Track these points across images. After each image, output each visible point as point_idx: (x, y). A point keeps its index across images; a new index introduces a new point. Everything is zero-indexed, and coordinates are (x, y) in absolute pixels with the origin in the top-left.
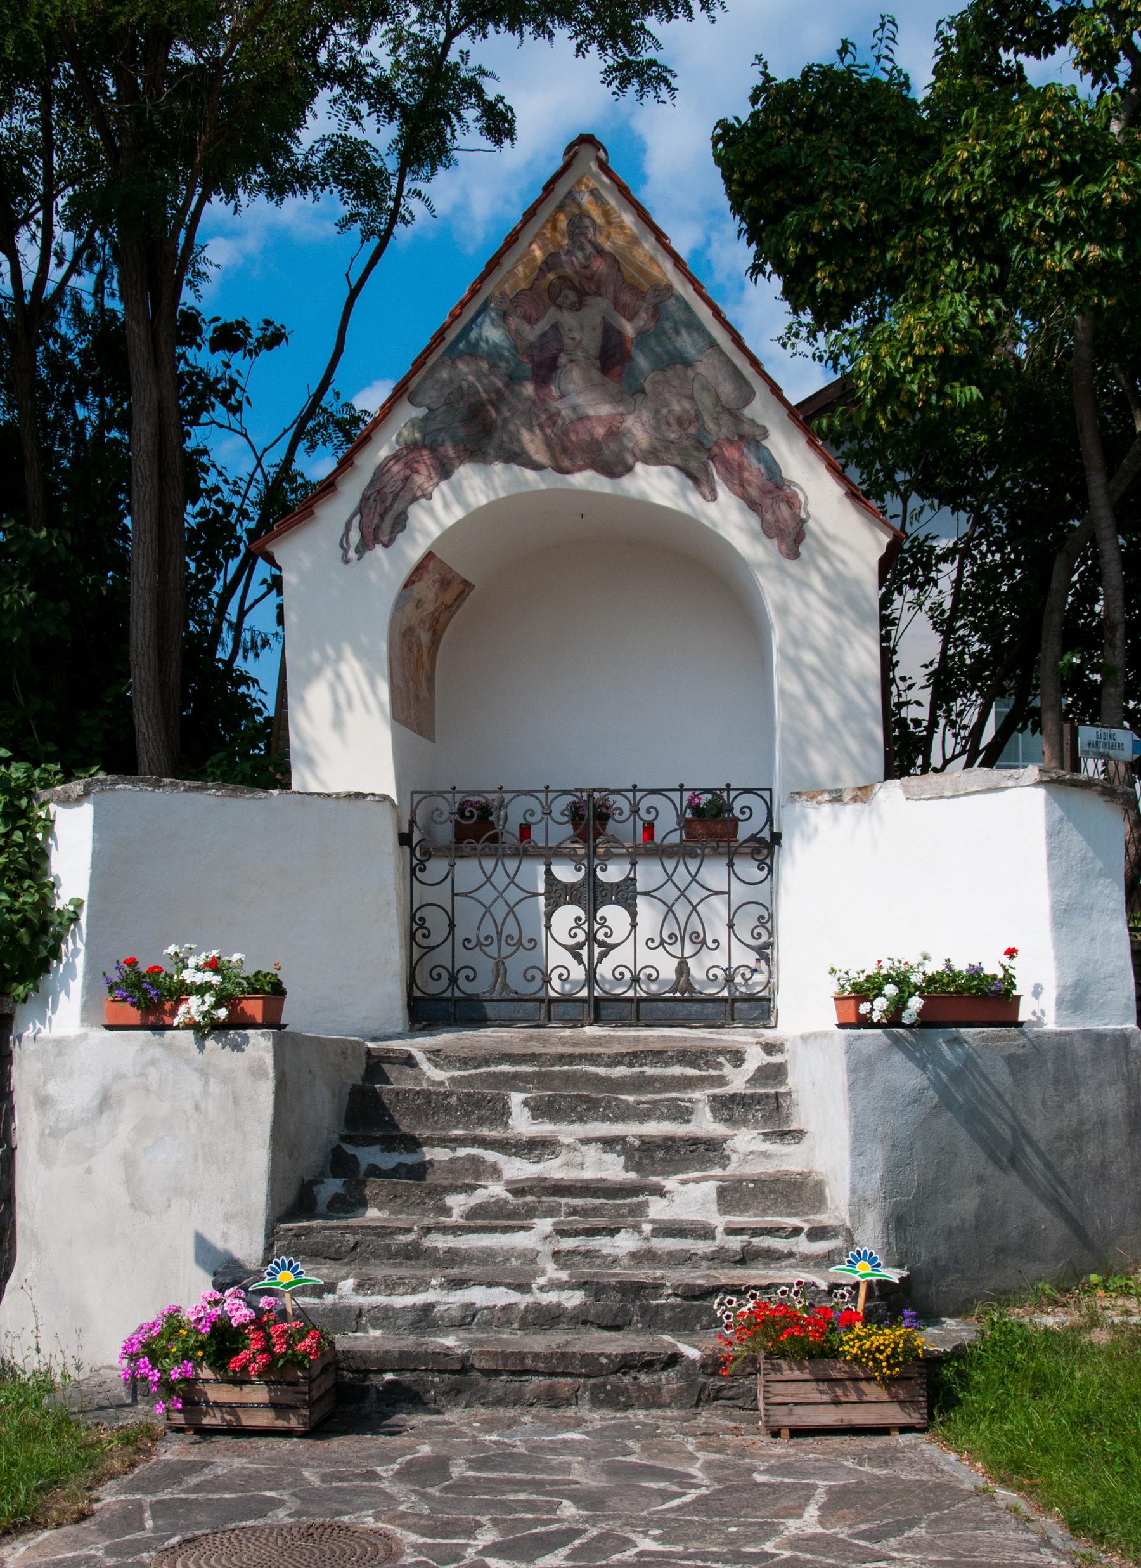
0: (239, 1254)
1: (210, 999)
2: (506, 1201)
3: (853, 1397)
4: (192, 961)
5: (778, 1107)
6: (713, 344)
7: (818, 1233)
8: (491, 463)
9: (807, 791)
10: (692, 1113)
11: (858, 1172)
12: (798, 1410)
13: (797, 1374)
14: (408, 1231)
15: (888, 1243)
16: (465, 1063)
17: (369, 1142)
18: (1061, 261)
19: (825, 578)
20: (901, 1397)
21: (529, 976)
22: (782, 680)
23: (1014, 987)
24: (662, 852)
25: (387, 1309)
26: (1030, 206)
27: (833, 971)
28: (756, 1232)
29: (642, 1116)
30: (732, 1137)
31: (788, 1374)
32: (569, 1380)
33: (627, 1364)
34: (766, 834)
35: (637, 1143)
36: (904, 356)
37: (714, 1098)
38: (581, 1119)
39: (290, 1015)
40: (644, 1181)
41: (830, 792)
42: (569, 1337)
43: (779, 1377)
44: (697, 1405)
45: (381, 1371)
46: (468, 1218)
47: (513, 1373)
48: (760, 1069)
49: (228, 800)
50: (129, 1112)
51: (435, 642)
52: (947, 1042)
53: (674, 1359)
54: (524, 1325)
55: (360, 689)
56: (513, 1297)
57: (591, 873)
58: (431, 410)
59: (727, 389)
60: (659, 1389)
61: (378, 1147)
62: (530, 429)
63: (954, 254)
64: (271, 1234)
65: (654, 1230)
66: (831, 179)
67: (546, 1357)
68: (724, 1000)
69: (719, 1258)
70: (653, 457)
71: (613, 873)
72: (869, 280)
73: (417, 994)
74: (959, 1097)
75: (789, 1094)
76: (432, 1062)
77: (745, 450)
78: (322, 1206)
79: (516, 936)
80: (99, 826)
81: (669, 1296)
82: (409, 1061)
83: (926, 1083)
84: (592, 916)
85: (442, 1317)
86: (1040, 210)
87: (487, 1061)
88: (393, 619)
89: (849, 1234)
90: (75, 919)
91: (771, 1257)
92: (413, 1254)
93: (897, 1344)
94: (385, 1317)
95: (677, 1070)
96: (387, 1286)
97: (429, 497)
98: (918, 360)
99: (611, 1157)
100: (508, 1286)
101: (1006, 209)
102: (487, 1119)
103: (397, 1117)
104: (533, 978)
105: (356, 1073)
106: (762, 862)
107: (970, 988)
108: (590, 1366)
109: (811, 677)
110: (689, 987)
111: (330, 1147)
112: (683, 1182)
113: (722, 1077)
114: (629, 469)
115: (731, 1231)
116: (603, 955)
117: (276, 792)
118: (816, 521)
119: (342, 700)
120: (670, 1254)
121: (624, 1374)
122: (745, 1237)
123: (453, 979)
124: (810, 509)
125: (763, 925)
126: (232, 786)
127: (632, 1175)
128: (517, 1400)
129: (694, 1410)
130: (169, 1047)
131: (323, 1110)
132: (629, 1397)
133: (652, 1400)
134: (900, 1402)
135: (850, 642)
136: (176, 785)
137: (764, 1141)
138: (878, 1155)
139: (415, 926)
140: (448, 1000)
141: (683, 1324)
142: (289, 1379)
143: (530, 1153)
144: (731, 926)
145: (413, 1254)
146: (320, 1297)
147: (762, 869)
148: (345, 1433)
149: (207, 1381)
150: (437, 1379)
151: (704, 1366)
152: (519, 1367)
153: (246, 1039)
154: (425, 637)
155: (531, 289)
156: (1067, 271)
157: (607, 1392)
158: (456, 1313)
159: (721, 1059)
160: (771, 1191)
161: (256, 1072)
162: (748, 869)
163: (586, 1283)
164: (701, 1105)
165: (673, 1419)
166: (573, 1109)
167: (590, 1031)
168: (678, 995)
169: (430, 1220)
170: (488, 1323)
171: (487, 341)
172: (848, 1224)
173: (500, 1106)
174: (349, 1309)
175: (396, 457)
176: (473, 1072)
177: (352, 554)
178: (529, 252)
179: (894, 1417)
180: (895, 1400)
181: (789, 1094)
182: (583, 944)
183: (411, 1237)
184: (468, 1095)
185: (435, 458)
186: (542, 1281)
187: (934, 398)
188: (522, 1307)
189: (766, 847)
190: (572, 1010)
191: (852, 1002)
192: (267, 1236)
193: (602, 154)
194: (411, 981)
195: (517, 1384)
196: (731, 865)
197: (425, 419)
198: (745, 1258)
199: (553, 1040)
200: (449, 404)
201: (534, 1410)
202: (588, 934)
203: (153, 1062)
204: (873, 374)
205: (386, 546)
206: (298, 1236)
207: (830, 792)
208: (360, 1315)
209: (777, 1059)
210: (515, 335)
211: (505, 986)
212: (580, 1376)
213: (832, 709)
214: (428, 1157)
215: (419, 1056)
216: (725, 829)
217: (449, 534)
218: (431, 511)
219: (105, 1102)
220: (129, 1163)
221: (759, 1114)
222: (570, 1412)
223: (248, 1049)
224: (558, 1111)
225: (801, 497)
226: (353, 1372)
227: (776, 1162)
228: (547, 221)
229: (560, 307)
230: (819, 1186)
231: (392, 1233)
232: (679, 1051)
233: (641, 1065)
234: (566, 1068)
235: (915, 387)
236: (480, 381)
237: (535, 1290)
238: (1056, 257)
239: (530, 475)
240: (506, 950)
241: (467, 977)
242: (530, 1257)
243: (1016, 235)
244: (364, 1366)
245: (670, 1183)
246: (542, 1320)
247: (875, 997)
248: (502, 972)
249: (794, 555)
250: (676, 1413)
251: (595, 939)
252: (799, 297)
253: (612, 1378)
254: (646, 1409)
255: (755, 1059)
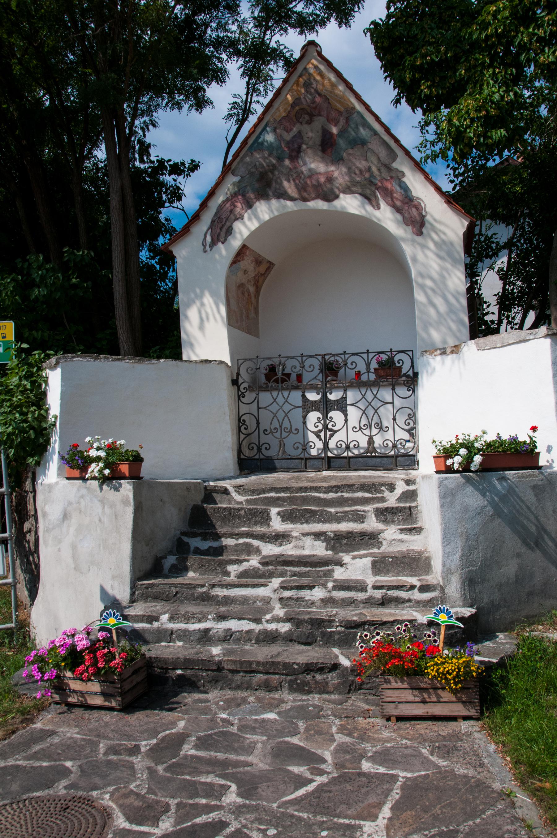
0: (118, 597)
1: (101, 465)
2: (258, 569)
3: (434, 699)
4: (96, 445)
5: (411, 514)
6: (376, 133)
7: (424, 588)
8: (270, 200)
9: (431, 350)
10: (365, 518)
11: (446, 555)
12: (401, 706)
13: (400, 685)
14: (203, 586)
15: (465, 594)
16: (253, 492)
17: (195, 535)
18: (548, 57)
19: (435, 243)
20: (464, 699)
21: (295, 447)
22: (419, 296)
23: (536, 447)
24: (369, 385)
25: (185, 631)
26: (531, 30)
27: (434, 442)
28: (390, 588)
29: (339, 519)
30: (383, 531)
31: (394, 685)
32: (277, 676)
33: (309, 668)
34: (411, 373)
35: (332, 535)
36: (465, 119)
37: (377, 510)
38: (307, 522)
39: (146, 470)
40: (337, 557)
41: (440, 349)
42: (280, 649)
43: (389, 686)
44: (349, 692)
45: (175, 669)
46: (239, 578)
47: (246, 672)
48: (403, 493)
49: (136, 365)
50: (74, 520)
51: (258, 292)
52: (498, 479)
53: (335, 666)
54: (258, 641)
55: (212, 310)
56: (252, 626)
57: (325, 396)
58: (242, 177)
59: (383, 153)
60: (327, 683)
61: (199, 538)
62: (289, 181)
63: (491, 66)
64: (133, 587)
65: (334, 586)
66: (427, 39)
67: (263, 663)
68: (392, 456)
69: (369, 602)
70: (348, 190)
71: (333, 396)
72: (448, 87)
73: (242, 457)
74: (506, 511)
75: (417, 507)
76: (237, 493)
77: (394, 184)
78: (166, 571)
79: (289, 427)
80: (64, 379)
81: (337, 626)
82: (225, 491)
83: (486, 503)
84: (325, 417)
85: (214, 636)
86: (536, 31)
87: (264, 491)
88: (228, 278)
89: (442, 589)
90: (54, 425)
91: (398, 601)
92: (206, 598)
93: (459, 669)
94: (184, 635)
95: (360, 494)
96: (185, 619)
97: (242, 218)
98: (472, 120)
99: (318, 543)
100: (249, 619)
101: (517, 34)
102: (259, 522)
103: (214, 521)
104: (298, 448)
105: (197, 498)
106: (409, 387)
107: (511, 449)
108: (288, 669)
109: (430, 292)
110: (374, 450)
111: (176, 538)
112: (354, 558)
113: (384, 497)
114: (337, 197)
115: (375, 587)
116: (331, 436)
117: (162, 361)
118: (432, 216)
119: (204, 316)
120: (343, 600)
121: (307, 674)
122: (384, 591)
123: (259, 450)
124: (427, 209)
125: (410, 418)
126: (138, 358)
127: (330, 552)
128: (247, 687)
129: (347, 696)
130: (88, 489)
131: (172, 518)
132: (310, 687)
133: (323, 689)
134: (464, 703)
135: (449, 274)
136: (108, 358)
137: (401, 533)
138: (458, 545)
139: (240, 423)
140: (257, 459)
141: (345, 642)
142: (110, 679)
143: (276, 541)
144: (394, 419)
145: (206, 598)
146: (151, 623)
147: (409, 391)
148: (145, 708)
149: (70, 678)
150: (204, 674)
151: (352, 671)
152: (249, 668)
153: (120, 485)
154: (252, 289)
155: (287, 116)
156: (552, 63)
157: (297, 684)
158: (221, 634)
159: (383, 488)
160: (401, 563)
161: (125, 502)
162: (402, 391)
163: (292, 619)
164: (370, 513)
165: (333, 702)
166: (303, 516)
167: (325, 473)
168: (369, 454)
169: (217, 580)
170: (239, 640)
171: (267, 141)
172: (441, 584)
173: (265, 515)
174: (166, 630)
175: (227, 200)
176: (257, 497)
177: (208, 248)
178: (286, 98)
179: (459, 711)
180: (459, 701)
181: (417, 507)
182: (321, 430)
183: (205, 589)
184: (250, 509)
185: (245, 199)
186: (268, 617)
187: (482, 139)
188: (257, 631)
189: (412, 381)
190: (317, 463)
191: (443, 459)
192: (131, 588)
193: (318, 49)
194: (240, 451)
195: (249, 678)
196: (393, 389)
197: (239, 182)
198: (384, 602)
199: (303, 479)
200: (251, 174)
201: (257, 693)
202: (323, 426)
203: (82, 497)
204: (449, 130)
205: (223, 243)
206: (147, 588)
207: (440, 349)
208: (172, 633)
209: (412, 488)
210: (279, 138)
211: (284, 452)
212: (283, 674)
213: (442, 307)
214: (224, 543)
215: (231, 489)
216: (395, 374)
217: (253, 234)
218: (244, 224)
219: (66, 516)
220: (74, 547)
221: (401, 518)
222: (277, 695)
223: (122, 490)
224: (295, 517)
225: (423, 205)
226: (160, 668)
227: (407, 545)
228: (294, 83)
229: (301, 123)
230: (428, 559)
231: (195, 587)
232: (361, 485)
233: (342, 492)
234: (303, 494)
235: (472, 135)
236: (265, 161)
237: (264, 622)
238: (546, 56)
239: (289, 203)
240: (284, 434)
241: (266, 448)
242: (267, 601)
243: (523, 48)
244: (167, 665)
245: (346, 558)
246: (267, 639)
247: (455, 455)
248: (282, 445)
249: (420, 233)
250: (337, 697)
251: (327, 428)
252: (414, 101)
253: (300, 676)
254: (320, 694)
255: (401, 488)
